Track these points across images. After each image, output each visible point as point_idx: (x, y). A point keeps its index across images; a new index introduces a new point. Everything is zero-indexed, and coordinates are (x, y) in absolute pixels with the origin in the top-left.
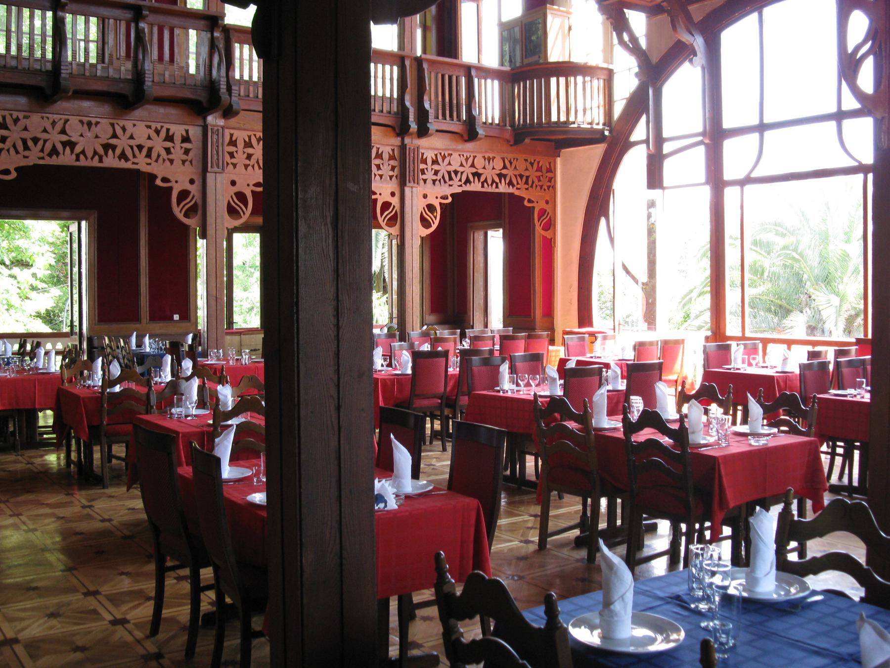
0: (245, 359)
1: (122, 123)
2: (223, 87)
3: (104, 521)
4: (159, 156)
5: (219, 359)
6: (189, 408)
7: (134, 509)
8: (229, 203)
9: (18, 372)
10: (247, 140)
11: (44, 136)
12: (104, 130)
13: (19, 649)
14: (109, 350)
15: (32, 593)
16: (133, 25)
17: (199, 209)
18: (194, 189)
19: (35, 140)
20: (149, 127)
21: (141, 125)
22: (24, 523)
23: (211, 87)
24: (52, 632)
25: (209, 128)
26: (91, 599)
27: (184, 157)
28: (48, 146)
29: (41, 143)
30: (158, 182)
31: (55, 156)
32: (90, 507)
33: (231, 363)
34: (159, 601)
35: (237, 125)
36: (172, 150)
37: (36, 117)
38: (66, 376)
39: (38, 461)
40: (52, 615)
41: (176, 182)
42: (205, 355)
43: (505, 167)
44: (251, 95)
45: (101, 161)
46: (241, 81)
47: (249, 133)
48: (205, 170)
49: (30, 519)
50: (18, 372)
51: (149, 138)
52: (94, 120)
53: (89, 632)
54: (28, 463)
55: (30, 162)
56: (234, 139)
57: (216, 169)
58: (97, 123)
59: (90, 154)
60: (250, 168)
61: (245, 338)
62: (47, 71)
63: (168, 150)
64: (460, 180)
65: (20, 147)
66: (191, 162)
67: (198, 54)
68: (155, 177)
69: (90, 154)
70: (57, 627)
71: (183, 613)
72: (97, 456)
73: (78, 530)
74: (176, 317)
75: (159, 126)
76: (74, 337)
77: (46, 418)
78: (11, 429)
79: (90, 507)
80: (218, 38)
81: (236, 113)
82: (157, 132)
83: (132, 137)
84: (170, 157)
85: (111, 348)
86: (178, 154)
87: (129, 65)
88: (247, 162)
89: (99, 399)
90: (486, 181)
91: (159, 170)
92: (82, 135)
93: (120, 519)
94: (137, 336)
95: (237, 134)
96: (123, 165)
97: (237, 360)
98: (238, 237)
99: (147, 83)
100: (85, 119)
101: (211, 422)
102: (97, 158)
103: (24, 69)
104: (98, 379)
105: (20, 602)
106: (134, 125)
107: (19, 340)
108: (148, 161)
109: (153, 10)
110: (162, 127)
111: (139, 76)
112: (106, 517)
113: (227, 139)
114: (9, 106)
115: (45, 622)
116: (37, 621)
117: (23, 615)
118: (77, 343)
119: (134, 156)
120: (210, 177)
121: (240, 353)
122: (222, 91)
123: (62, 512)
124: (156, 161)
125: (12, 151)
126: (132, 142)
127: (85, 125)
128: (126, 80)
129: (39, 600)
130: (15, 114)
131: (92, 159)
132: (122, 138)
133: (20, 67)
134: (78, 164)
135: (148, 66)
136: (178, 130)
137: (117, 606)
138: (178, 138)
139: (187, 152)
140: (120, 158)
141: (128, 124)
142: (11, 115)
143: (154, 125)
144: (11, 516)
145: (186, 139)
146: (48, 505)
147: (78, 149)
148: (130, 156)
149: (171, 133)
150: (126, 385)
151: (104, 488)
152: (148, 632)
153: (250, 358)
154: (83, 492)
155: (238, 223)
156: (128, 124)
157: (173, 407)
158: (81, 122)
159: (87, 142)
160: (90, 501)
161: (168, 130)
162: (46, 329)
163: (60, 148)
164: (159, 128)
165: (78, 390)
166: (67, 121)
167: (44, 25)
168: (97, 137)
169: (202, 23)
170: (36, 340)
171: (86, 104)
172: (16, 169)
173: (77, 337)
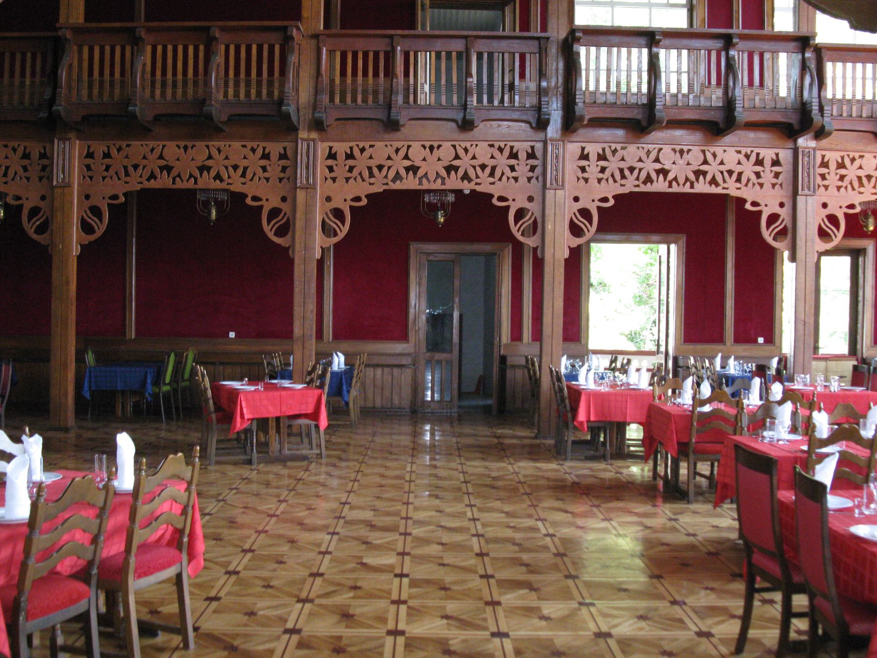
0: (835, 387)
1: (712, 149)
2: (815, 108)
3: (688, 535)
4: (748, 180)
5: (805, 385)
6: (780, 434)
7: (717, 527)
8: (571, 221)
9: (611, 387)
10: (840, 161)
11: (639, 165)
12: (695, 157)
13: (612, 642)
14: (694, 370)
15: (622, 594)
16: (723, 53)
17: (788, 233)
18: (784, 213)
19: (632, 169)
20: (739, 152)
21: (731, 151)
22: (615, 528)
23: (803, 110)
24: (642, 633)
25: (800, 150)
26: (677, 608)
27: (775, 181)
28: (643, 175)
29: (636, 172)
30: (748, 206)
31: (649, 184)
32: (675, 520)
33: (819, 389)
34: (746, 619)
35: (829, 146)
36: (762, 173)
37: (632, 148)
38: (657, 393)
39: (625, 471)
40: (641, 618)
41: (766, 205)
42: (791, 379)
43: (457, 157)
44: (845, 114)
45: (692, 187)
46: (832, 101)
47: (842, 154)
48: (795, 193)
49: (620, 526)
50: (611, 387)
51: (739, 163)
52: (685, 148)
53: (676, 640)
54: (617, 473)
55: (378, 188)
56: (826, 160)
57: (806, 192)
58: (689, 151)
59: (681, 180)
60: (842, 190)
61: (832, 364)
62: (643, 105)
63: (758, 175)
64: (386, 177)
65: (618, 176)
66: (781, 185)
67: (789, 76)
68: (744, 201)
69: (681, 180)
70: (645, 630)
71: (770, 636)
72: (683, 471)
73: (664, 541)
74: (761, 340)
75: (749, 150)
76: (660, 355)
77: (634, 432)
78: (602, 439)
79: (675, 520)
80: (809, 58)
81: (829, 134)
82: (747, 157)
83: (722, 163)
84: (760, 181)
85: (696, 368)
86: (767, 177)
87: (719, 92)
88: (840, 183)
89: (688, 418)
90: (179, 176)
91: (748, 194)
92: (674, 163)
93: (704, 535)
94: (722, 357)
95: (829, 155)
96: (714, 190)
97: (825, 386)
98: (827, 262)
99: (737, 109)
100: (678, 148)
101: (805, 448)
102: (688, 184)
103: (622, 104)
104: (686, 399)
105: (613, 600)
106: (725, 151)
107: (610, 356)
108: (738, 185)
109: (743, 37)
110: (752, 151)
111: (729, 105)
112: (691, 531)
113: (819, 160)
114: (608, 139)
115: (635, 623)
116: (628, 620)
117: (615, 612)
118: (663, 362)
119: (724, 181)
120: (800, 200)
121: (827, 379)
122: (814, 112)
123: (648, 522)
124: (746, 185)
125: (611, 180)
126: (722, 168)
127: (678, 153)
128: (718, 108)
129: (628, 601)
130: (613, 146)
131: (684, 185)
132: (713, 164)
133: (618, 103)
134: (670, 190)
135: (738, 92)
136: (768, 154)
137: (702, 618)
138: (767, 162)
139: (777, 175)
140: (710, 183)
141: (719, 150)
142: (610, 147)
143: (497, 144)
144: (603, 520)
145: (776, 163)
146: (637, 514)
147: (671, 176)
148: (225, 176)
149: (333, 151)
150: (716, 405)
151: (688, 503)
152: (733, 649)
153: (839, 385)
154: (668, 506)
155: (829, 246)
156: (719, 150)
157: (765, 430)
158: (424, 147)
159: (679, 169)
160: (675, 514)
161: (758, 154)
162: (631, 347)
163: (654, 175)
164: (749, 153)
165: (668, 406)
166: (660, 150)
167: (640, 62)
168: (688, 164)
169: (792, 45)
170: (626, 357)
171: (678, 133)
172: (614, 197)
173: (663, 356)
